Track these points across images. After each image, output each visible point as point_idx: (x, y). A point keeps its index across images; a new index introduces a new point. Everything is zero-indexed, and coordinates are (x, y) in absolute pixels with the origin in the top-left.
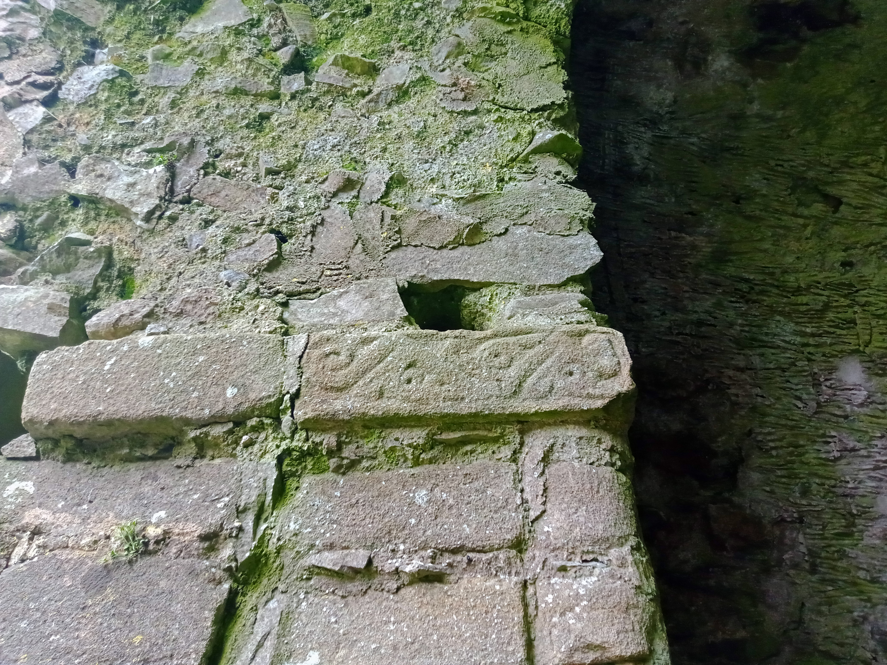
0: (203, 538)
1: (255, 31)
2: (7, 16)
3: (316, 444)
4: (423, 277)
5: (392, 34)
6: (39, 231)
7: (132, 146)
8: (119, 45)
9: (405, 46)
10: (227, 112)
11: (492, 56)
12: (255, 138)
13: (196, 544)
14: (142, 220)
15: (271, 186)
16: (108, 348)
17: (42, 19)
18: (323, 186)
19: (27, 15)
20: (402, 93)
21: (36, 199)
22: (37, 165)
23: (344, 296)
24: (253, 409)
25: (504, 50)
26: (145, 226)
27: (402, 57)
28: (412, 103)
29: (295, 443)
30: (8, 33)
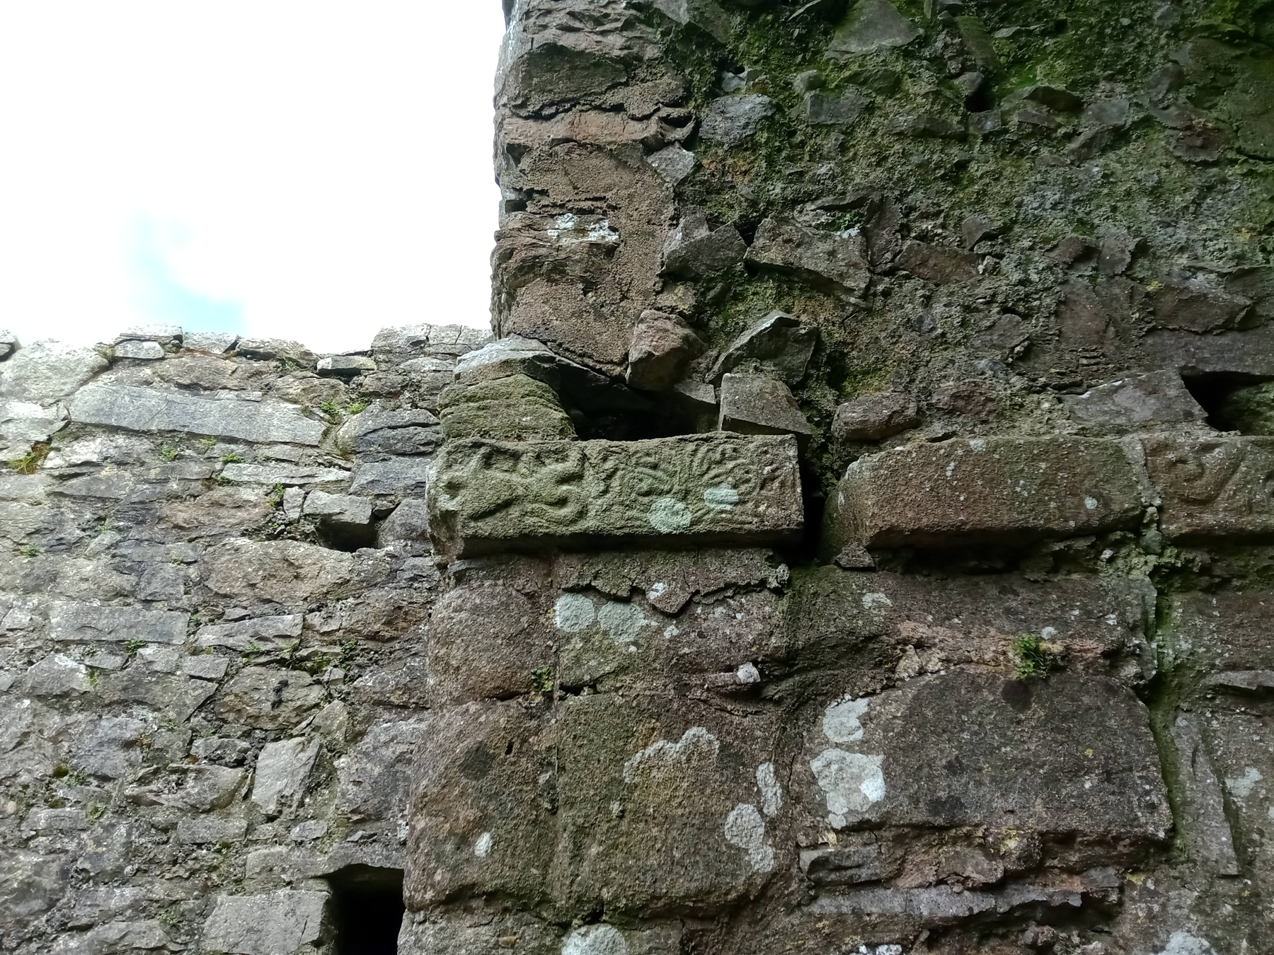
0: (1105, 655)
1: (927, 53)
2: (623, 29)
3: (1188, 561)
4: (1193, 368)
5: (1094, 59)
6: (711, 306)
7: (804, 202)
8: (758, 68)
9: (1112, 75)
10: (915, 159)
11: (1219, 88)
12: (953, 193)
13: (1101, 661)
14: (860, 297)
15: (989, 254)
16: (942, 451)
17: (664, 34)
18: (1052, 255)
19: (643, 27)
20: (1120, 136)
21: (710, 267)
22: (706, 226)
23: (1121, 391)
24: (1117, 521)
25: (1231, 80)
26: (863, 304)
27: (1112, 90)
28: (1134, 148)
29: (1165, 560)
30: (626, 52)
